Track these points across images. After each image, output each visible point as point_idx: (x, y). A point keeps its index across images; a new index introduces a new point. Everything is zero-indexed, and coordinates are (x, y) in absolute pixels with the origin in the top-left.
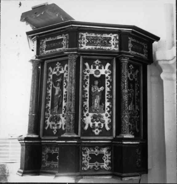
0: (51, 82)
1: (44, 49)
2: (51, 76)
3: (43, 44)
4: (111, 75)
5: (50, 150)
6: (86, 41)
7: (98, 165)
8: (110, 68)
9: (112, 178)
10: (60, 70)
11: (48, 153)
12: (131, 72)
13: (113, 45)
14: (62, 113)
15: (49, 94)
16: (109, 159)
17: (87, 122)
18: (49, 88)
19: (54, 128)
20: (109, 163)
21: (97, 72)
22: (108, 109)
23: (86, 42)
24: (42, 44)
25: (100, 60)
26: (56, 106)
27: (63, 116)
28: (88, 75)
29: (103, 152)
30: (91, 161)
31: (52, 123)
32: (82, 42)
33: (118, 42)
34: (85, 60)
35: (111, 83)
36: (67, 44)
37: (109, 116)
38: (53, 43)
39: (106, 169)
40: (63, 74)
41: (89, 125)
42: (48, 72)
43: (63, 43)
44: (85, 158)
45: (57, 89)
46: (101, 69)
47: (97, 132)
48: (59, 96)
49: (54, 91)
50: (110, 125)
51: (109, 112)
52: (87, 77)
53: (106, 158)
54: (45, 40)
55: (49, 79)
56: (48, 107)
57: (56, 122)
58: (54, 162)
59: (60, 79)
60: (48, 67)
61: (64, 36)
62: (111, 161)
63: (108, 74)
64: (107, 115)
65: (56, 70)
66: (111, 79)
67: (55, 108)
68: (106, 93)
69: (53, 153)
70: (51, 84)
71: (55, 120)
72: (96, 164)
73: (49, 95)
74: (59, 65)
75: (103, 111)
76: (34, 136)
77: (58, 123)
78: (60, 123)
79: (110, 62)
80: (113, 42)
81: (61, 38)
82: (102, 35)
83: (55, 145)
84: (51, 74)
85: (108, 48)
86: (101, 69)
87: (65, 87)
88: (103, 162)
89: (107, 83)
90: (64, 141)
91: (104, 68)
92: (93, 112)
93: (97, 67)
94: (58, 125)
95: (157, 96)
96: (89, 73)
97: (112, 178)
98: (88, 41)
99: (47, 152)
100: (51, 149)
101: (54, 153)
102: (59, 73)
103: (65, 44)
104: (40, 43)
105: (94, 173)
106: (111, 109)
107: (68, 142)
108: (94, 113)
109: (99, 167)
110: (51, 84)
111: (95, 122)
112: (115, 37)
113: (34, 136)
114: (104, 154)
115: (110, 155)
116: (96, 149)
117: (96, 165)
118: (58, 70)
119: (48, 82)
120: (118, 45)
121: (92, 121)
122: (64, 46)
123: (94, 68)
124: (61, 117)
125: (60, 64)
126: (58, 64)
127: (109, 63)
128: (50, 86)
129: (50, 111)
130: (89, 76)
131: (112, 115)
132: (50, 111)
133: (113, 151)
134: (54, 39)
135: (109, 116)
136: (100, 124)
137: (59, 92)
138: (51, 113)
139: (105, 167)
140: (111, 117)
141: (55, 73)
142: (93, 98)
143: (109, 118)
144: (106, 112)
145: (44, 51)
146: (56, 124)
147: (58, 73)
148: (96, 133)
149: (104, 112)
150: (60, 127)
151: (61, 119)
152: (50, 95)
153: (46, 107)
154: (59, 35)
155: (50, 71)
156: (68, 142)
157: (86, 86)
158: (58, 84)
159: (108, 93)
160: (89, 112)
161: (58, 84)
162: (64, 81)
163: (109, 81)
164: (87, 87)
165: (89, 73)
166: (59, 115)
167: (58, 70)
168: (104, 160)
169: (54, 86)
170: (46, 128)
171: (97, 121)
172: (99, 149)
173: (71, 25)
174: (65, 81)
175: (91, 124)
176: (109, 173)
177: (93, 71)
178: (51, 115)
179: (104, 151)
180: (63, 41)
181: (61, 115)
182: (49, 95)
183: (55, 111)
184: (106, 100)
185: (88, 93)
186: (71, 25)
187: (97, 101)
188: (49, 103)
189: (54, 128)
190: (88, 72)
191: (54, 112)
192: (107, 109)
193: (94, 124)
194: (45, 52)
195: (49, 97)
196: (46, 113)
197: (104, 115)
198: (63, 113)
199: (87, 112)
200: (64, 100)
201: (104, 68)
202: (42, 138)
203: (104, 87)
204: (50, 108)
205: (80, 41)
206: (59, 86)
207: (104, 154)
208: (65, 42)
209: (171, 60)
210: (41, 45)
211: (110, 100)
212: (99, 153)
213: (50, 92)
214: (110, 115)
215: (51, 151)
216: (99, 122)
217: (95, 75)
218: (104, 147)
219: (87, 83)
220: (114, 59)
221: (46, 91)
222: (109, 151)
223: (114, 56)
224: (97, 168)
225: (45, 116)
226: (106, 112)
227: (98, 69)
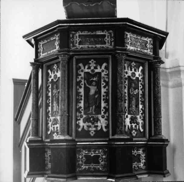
0: (83, 81)
1: (76, 43)
2: (82, 74)
3: (75, 37)
4: (143, 78)
5: (88, 152)
6: (130, 42)
7: (137, 165)
8: (143, 71)
9: (149, 176)
10: (96, 68)
11: (84, 155)
12: (133, 69)
13: (149, 49)
14: (101, 114)
15: (80, 93)
16: (144, 159)
17: (127, 124)
18: (81, 87)
19: (90, 129)
20: (144, 162)
21: (134, 74)
22: (142, 112)
23: (130, 43)
24: (73, 37)
25: (135, 62)
26: (92, 107)
27: (103, 117)
28: (127, 76)
29: (140, 153)
30: (86, 163)
31: (87, 124)
32: (127, 42)
33: (152, 46)
34: (78, 61)
35: (107, 83)
36: (111, 42)
37: (142, 118)
38: (91, 38)
39: (142, 168)
40: (100, 74)
41: (128, 126)
42: (78, 68)
43: (106, 39)
44: (80, 160)
45: (93, 90)
46: (136, 71)
47: (134, 133)
48: (96, 96)
49: (87, 90)
50: (144, 126)
51: (142, 114)
52: (126, 79)
53: (142, 158)
54: (77, 32)
55: (80, 77)
56: (81, 107)
57: (93, 124)
58: (95, 165)
59: (97, 78)
60: (77, 63)
61: (107, 32)
62: (146, 161)
63: (141, 77)
64: (140, 118)
65: (89, 68)
66: (143, 83)
67: (91, 108)
68: (140, 96)
69: (92, 155)
70: (83, 83)
71: (93, 121)
72: (92, 166)
73: (81, 94)
74: (94, 63)
75: (138, 113)
76: (67, 137)
77: (96, 125)
78: (99, 124)
79: (107, 61)
80: (76, 39)
81: (102, 33)
82: (141, 37)
83: (96, 147)
84: (82, 71)
85: (146, 51)
86: (136, 71)
87: (103, 87)
88: (140, 162)
89: (140, 87)
90: (122, 142)
91: (101, 68)
92: (131, 114)
93: (133, 69)
94: (96, 127)
95: (159, 100)
96: (127, 75)
97: (149, 176)
98: (131, 42)
99: (84, 154)
100: (89, 151)
101: (94, 155)
102: (94, 71)
103: (108, 41)
104: (70, 36)
105: (90, 174)
106: (144, 112)
107: (126, 143)
108: (132, 115)
109: (138, 166)
110: (83, 83)
111: (133, 124)
112: (150, 41)
113: (67, 137)
114: (140, 154)
115: (144, 155)
116: (135, 149)
117: (136, 165)
118: (92, 68)
119: (78, 80)
120: (152, 50)
121: (131, 123)
122: (107, 43)
123: (131, 70)
124: (100, 118)
125: (95, 62)
126: (92, 62)
127: (106, 63)
128: (81, 84)
129: (82, 112)
130: (127, 77)
131: (144, 117)
132: (82, 112)
133: (146, 151)
134: (92, 34)
135: (142, 118)
136: (136, 126)
137: (96, 93)
138: (84, 114)
139: (142, 167)
140: (144, 120)
141: (86, 70)
142: (130, 100)
143: (142, 120)
144: (140, 115)
145: (77, 45)
146: (93, 126)
147: (93, 71)
148: (92, 135)
149: (138, 114)
150: (99, 128)
151: (100, 120)
152: (82, 94)
153: (78, 107)
154: (100, 30)
155: (80, 68)
156: (126, 143)
157: (49, 91)
158: (94, 83)
159: (141, 96)
160: (128, 114)
161: (94, 83)
162: (102, 80)
163: (141, 84)
164: (126, 88)
165: (127, 75)
166: (96, 115)
167: (92, 68)
168: (141, 160)
169: (87, 84)
170: (80, 130)
171: (134, 123)
172: (137, 151)
173: (125, 23)
174: (103, 81)
175: (130, 125)
176: (145, 172)
177: (130, 72)
178: (84, 116)
179: (141, 152)
180: (106, 38)
181: (100, 117)
182: (81, 94)
183: (90, 112)
184: (140, 103)
185: (50, 98)
186: (125, 23)
187: (134, 102)
188: (80, 103)
189: (90, 129)
190: (127, 73)
191: (90, 112)
192: (141, 111)
193: (132, 126)
194: (79, 47)
195: (82, 96)
196: (78, 113)
197: (138, 117)
198: (102, 113)
199: (127, 114)
200: (103, 100)
201: (138, 71)
202: (76, 140)
203: (139, 90)
204: (83, 108)
205: (112, 39)
206: (95, 86)
207: (140, 154)
208: (107, 39)
209: (169, 69)
210: (71, 38)
211: (143, 103)
212: (137, 153)
213: (82, 91)
214: (143, 117)
215: (90, 154)
216: (135, 124)
217: (132, 77)
218: (140, 148)
219: (126, 85)
220: (146, 63)
221: (77, 90)
222: (143, 151)
223: (148, 60)
224: (136, 168)
225: (76, 117)
226: (140, 115)
227: (134, 72)
